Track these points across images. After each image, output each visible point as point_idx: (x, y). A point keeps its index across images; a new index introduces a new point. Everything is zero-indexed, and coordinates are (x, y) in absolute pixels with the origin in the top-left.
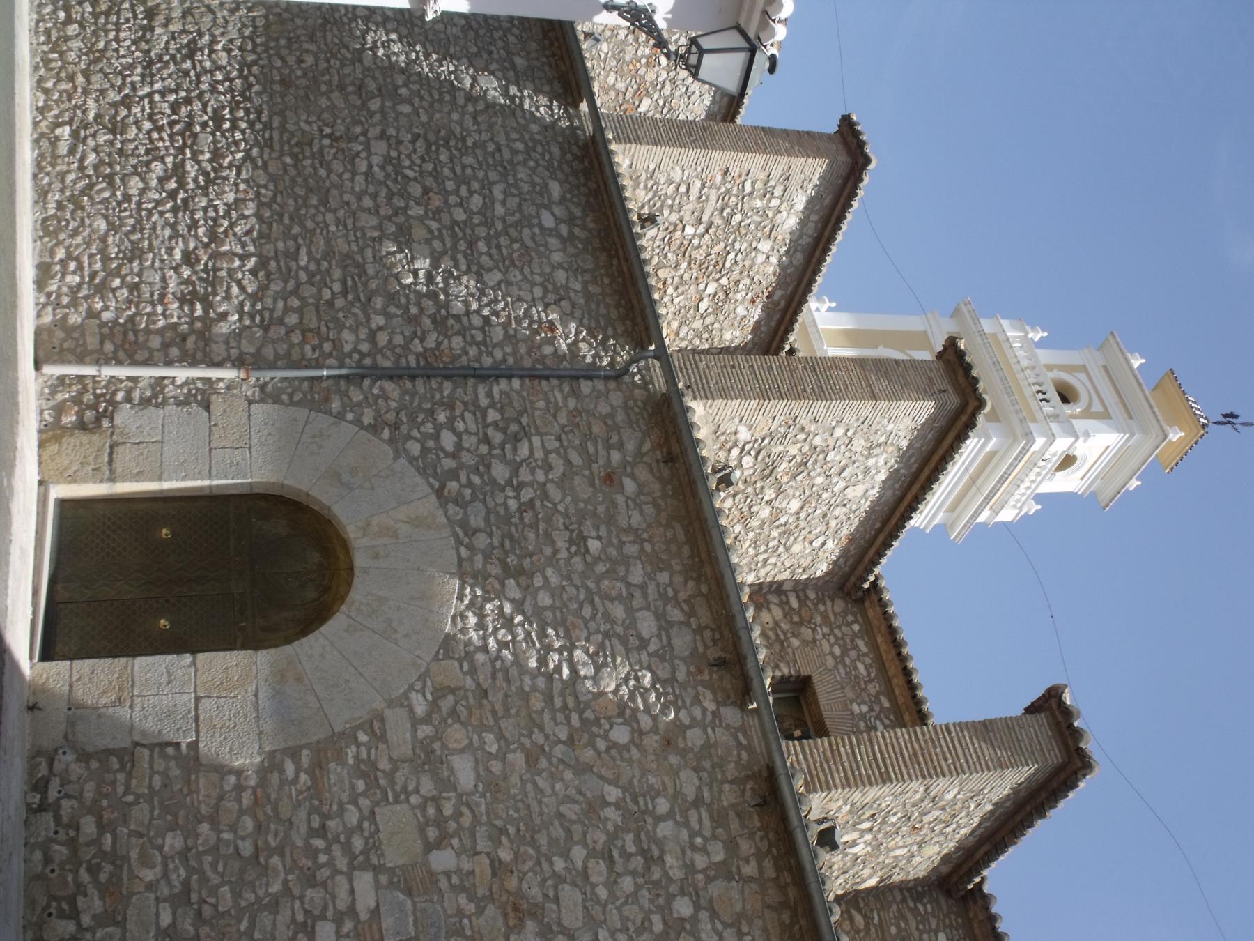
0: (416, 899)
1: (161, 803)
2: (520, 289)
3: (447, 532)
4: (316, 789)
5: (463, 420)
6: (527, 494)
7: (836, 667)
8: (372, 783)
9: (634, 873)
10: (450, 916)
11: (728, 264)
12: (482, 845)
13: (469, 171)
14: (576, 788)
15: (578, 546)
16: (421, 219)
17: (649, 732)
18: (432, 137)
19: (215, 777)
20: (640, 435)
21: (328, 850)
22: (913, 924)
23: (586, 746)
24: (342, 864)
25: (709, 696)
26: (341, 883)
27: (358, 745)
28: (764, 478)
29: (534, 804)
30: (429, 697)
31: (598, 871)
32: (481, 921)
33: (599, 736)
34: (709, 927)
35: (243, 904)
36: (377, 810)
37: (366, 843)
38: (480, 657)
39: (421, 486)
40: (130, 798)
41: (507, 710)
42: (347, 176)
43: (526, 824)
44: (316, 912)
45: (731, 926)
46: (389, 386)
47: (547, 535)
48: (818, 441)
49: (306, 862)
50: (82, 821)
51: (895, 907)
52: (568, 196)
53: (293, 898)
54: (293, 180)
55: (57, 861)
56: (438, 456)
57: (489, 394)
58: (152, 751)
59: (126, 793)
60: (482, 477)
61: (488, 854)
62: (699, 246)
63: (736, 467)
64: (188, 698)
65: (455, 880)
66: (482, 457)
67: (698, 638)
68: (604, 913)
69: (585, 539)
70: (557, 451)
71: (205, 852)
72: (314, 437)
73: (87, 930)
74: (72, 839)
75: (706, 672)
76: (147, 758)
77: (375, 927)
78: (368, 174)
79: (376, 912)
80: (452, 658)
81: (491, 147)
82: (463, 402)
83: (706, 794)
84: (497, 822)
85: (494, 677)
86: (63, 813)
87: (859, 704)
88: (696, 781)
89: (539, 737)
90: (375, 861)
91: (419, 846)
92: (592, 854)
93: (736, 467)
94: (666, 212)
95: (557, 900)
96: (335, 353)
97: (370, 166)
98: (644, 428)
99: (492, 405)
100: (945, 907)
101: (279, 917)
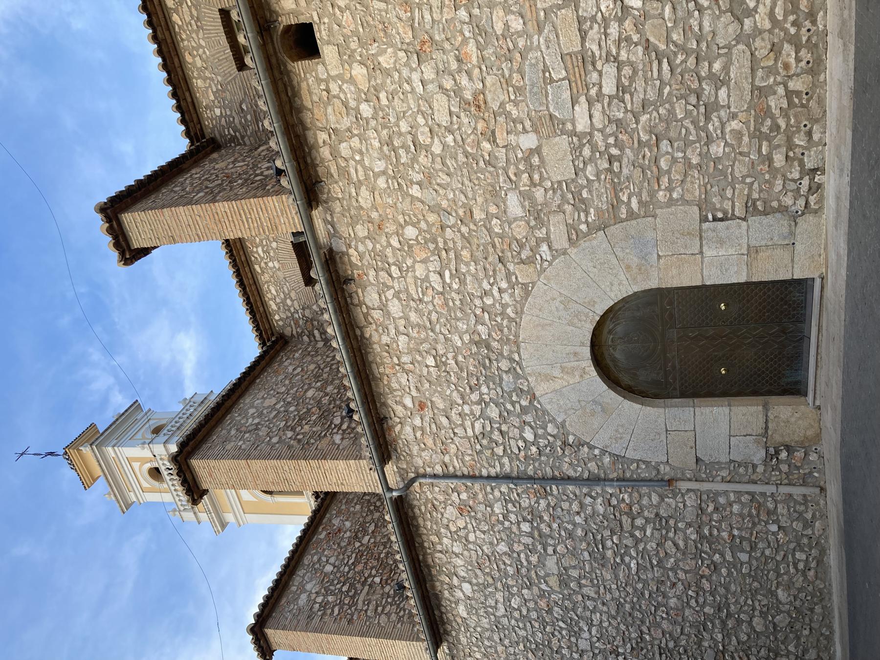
0: (547, 112)
1: (726, 177)
2: (484, 539)
3: (528, 370)
4: (616, 190)
5: (519, 448)
6: (475, 397)
7: (290, 292)
8: (577, 195)
9: (400, 134)
10: (523, 101)
11: (354, 555)
12: (501, 153)
13: (521, 625)
14: (439, 195)
15: (441, 361)
16: (553, 591)
17: (393, 234)
18: (547, 651)
19: (688, 197)
20: (402, 437)
21: (608, 146)
22: (237, 121)
23: (433, 224)
24: (598, 137)
25: (353, 259)
26: (598, 122)
27: (587, 222)
28: (328, 410)
29: (467, 182)
30: (538, 257)
31: (423, 138)
32: (502, 97)
33: (424, 231)
34: (349, 96)
35: (667, 106)
36: (574, 176)
37: (580, 153)
38: (504, 285)
39: (546, 403)
40: (748, 180)
41: (485, 248)
42: (605, 624)
43: (472, 168)
44: (616, 101)
45: (334, 97)
46: (571, 473)
47: (462, 370)
48: (290, 434)
49: (623, 137)
50: (784, 163)
51: (249, 133)
52: (453, 605)
53: (632, 111)
54: (643, 622)
55: (802, 133)
56: (535, 423)
57: (502, 465)
58: (733, 214)
59: (752, 183)
60: (505, 408)
61: (498, 146)
62: (371, 569)
63: (345, 417)
64: (708, 252)
65: (520, 127)
66: (505, 422)
67: (361, 299)
68: (419, 105)
69: (437, 366)
70: (457, 426)
71: (694, 142)
72: (621, 438)
73: (780, 83)
74: (791, 150)
75: (356, 276)
76: (736, 209)
77: (575, 91)
78: (591, 625)
79: (574, 102)
80: (522, 284)
81: (506, 642)
82: (520, 460)
83: (353, 190)
84: (492, 169)
85: (494, 271)
86: (798, 168)
87: (275, 267)
88: (360, 199)
89: (464, 229)
90: (575, 139)
91: (545, 151)
92: (427, 148)
93: (345, 417)
94: (392, 592)
95: (451, 114)
96: (609, 497)
97: (590, 631)
98: (400, 442)
99: (500, 458)
100: (216, 132)
101: (642, 96)
